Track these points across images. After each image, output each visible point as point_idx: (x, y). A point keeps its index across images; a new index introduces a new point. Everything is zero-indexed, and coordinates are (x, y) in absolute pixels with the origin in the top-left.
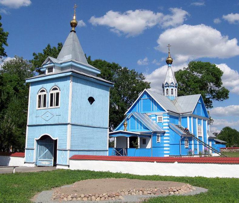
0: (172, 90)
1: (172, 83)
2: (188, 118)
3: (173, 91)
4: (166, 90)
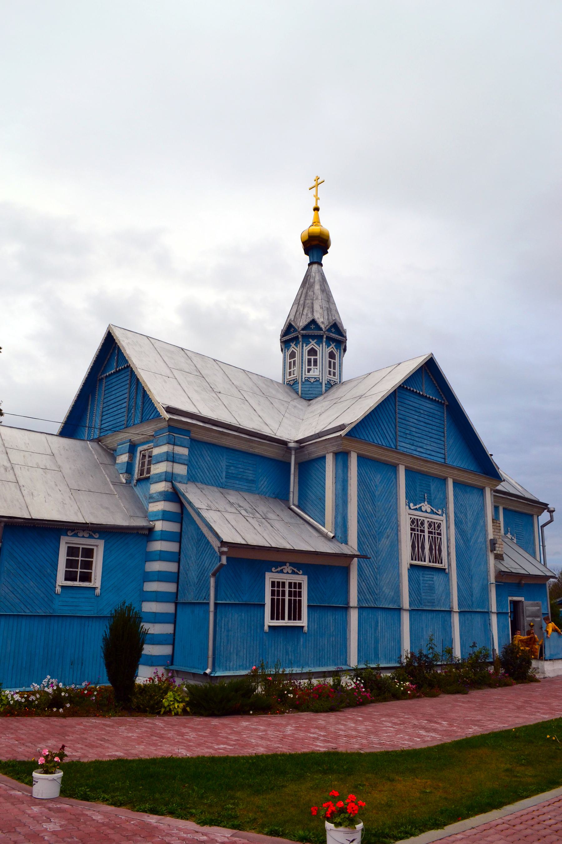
0: (312, 352)
3: (319, 357)
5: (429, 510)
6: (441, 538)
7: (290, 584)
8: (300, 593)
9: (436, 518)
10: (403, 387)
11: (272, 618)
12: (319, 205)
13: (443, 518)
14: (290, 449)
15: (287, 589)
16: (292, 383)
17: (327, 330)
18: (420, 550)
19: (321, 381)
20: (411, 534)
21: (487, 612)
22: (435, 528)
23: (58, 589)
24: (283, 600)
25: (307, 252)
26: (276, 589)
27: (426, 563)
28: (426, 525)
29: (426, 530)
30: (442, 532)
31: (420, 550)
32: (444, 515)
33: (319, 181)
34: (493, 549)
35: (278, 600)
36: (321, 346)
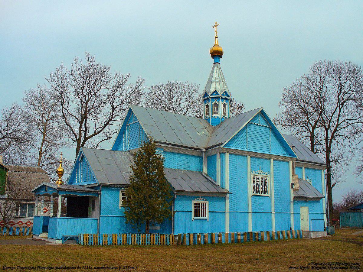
0: (216, 105)
1: (215, 91)
2: (218, 155)
4: (205, 107)
5: (262, 173)
6: (267, 184)
7: (202, 204)
8: (195, 207)
9: (264, 176)
10: (250, 123)
11: (195, 216)
12: (218, 36)
13: (269, 175)
14: (202, 152)
15: (200, 206)
16: (207, 118)
17: (222, 95)
18: (264, 188)
19: (219, 117)
20: (253, 183)
21: (225, 212)
22: (264, 181)
23: (193, 219)
24: (199, 210)
25: (213, 57)
26: (196, 206)
27: (261, 194)
28: (260, 179)
29: (260, 181)
30: (268, 181)
31: (264, 188)
32: (269, 174)
33: (217, 24)
34: (292, 187)
35: (197, 210)
36: (219, 102)
